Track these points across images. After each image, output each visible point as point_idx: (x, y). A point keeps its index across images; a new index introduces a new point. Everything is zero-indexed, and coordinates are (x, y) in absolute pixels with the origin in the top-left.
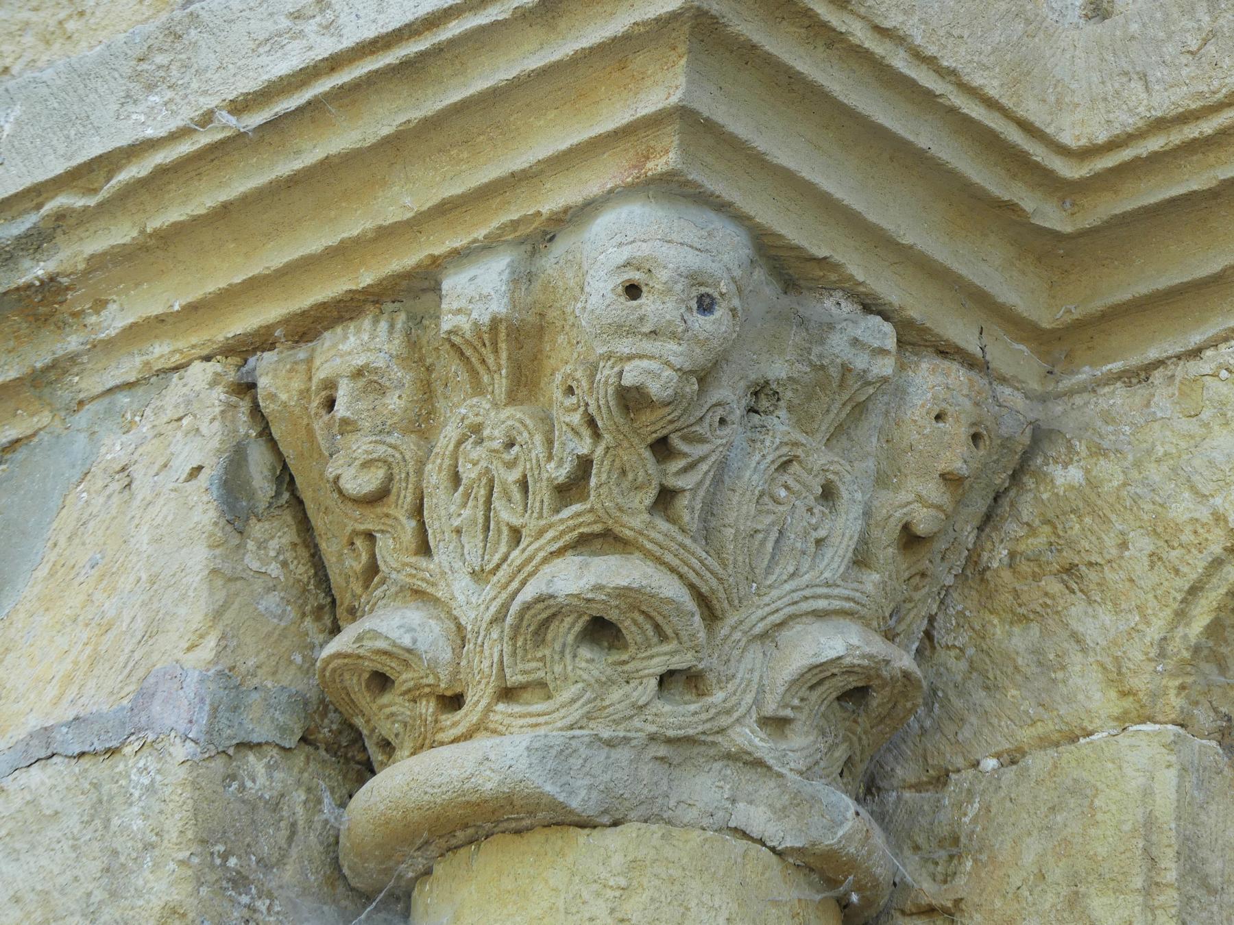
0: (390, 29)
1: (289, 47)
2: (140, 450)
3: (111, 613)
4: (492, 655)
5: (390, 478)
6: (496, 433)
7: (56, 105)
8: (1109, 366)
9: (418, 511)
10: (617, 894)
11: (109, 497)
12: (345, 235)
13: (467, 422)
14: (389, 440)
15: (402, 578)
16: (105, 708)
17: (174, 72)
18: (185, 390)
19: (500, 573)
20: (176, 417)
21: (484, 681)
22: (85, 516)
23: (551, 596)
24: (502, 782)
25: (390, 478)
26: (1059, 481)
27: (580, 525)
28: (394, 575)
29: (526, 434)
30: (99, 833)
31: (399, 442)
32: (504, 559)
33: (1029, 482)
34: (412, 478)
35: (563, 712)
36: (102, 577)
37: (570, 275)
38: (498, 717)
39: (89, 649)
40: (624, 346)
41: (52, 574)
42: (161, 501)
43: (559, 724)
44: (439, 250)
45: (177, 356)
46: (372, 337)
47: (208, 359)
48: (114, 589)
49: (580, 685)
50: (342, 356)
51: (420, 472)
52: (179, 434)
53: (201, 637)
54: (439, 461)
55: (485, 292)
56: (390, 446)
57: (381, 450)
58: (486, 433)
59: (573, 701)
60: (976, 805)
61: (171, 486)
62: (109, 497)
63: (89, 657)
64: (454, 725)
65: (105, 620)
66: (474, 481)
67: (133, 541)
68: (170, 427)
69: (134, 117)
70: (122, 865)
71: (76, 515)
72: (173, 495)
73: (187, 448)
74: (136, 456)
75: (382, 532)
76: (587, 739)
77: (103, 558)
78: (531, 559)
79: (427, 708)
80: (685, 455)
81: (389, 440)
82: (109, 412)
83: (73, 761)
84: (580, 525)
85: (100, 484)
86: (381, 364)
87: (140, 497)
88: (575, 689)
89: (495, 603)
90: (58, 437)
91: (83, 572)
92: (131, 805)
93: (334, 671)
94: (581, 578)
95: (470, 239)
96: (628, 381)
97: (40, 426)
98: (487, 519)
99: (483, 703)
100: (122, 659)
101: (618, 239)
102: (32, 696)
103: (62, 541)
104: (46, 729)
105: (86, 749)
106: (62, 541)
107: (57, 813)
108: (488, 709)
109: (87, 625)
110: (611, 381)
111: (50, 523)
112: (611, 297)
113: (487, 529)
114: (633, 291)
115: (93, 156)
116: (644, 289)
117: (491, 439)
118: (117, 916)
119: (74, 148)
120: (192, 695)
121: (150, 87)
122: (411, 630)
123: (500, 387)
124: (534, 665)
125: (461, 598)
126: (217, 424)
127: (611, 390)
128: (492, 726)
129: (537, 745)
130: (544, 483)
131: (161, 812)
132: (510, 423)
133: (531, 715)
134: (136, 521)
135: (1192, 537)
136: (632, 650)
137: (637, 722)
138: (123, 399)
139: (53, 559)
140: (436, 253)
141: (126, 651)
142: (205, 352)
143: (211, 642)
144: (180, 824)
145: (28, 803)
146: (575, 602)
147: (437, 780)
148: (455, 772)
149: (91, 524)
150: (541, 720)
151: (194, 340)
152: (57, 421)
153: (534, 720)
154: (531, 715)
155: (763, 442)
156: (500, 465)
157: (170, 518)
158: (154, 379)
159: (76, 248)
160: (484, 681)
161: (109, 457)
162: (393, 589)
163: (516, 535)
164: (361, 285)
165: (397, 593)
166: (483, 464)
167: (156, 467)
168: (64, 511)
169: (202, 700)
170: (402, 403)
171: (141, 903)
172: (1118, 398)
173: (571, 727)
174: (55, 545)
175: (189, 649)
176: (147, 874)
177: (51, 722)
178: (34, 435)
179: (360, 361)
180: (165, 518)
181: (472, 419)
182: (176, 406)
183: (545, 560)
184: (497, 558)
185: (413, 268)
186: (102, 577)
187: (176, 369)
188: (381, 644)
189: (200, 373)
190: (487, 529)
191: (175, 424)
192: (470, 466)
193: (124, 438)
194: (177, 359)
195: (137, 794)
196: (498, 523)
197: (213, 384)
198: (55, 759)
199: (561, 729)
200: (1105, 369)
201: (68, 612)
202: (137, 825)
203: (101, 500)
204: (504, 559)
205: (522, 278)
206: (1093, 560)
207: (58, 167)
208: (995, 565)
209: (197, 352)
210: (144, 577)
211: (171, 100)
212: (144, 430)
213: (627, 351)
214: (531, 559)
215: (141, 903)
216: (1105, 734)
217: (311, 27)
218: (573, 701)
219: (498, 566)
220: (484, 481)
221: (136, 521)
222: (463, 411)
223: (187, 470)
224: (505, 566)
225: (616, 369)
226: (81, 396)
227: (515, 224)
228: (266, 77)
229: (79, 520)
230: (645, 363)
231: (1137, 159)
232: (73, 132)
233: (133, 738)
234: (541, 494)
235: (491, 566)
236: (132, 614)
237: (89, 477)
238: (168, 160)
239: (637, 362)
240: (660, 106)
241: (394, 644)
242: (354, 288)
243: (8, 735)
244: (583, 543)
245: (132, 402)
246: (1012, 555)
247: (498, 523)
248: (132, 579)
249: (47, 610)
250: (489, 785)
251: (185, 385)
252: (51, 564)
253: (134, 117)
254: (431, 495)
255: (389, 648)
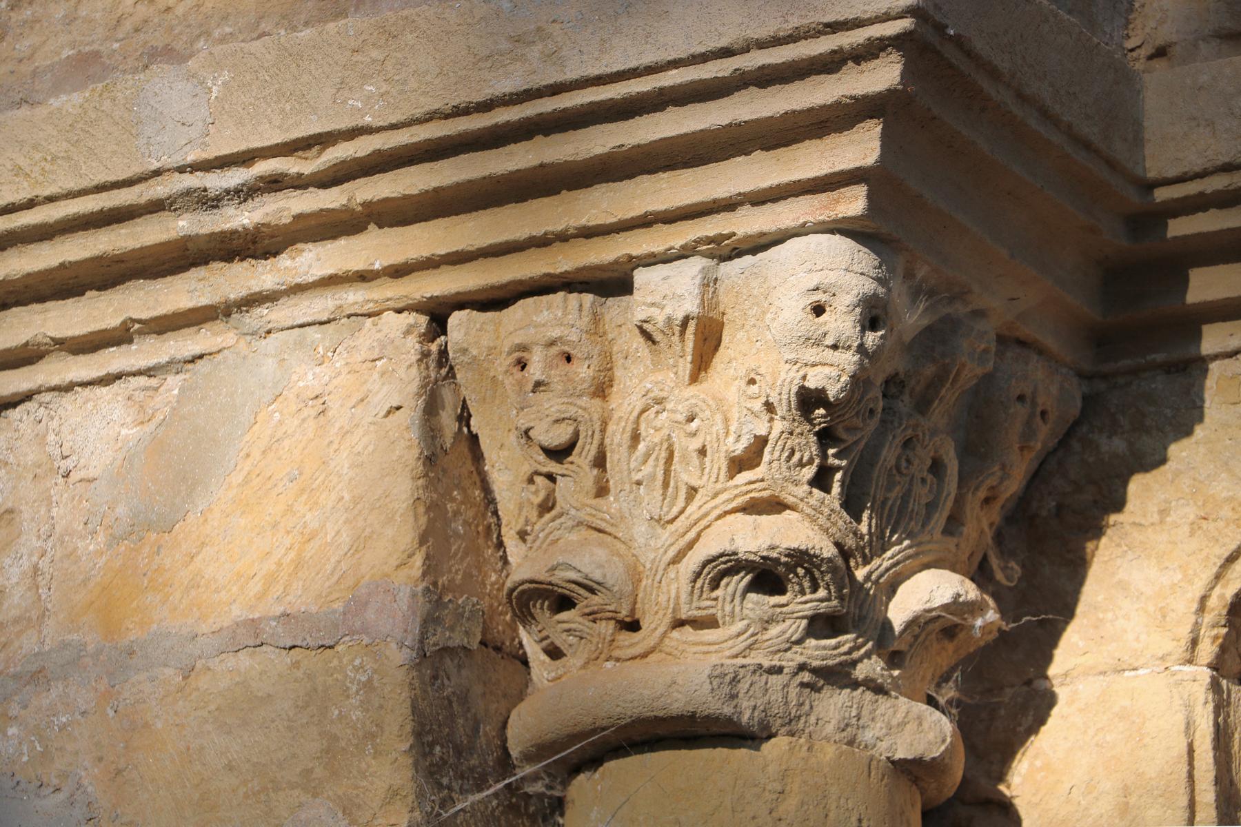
0: (615, 70)
1: (511, 68)
2: (335, 382)
3: (314, 525)
4: (669, 591)
5: (576, 434)
6: (680, 407)
7: (268, 78)
8: (1153, 356)
9: (600, 461)
10: (774, 797)
11: (304, 420)
12: (550, 228)
13: (652, 395)
14: (579, 402)
15: (582, 515)
16: (314, 609)
17: (390, 68)
18: (379, 335)
19: (678, 523)
20: (372, 357)
21: (661, 613)
22: (279, 434)
23: (735, 553)
24: (688, 703)
25: (576, 434)
26: (1104, 448)
27: (751, 491)
28: (573, 512)
29: (708, 413)
30: (316, 719)
31: (588, 405)
32: (682, 512)
33: (1076, 445)
34: (597, 436)
35: (730, 643)
36: (302, 491)
37: (754, 284)
38: (674, 644)
39: (292, 555)
40: (810, 354)
41: (246, 481)
42: (360, 431)
43: (727, 653)
44: (636, 252)
45: (371, 305)
46: (565, 314)
47: (399, 311)
48: (316, 503)
49: (745, 622)
50: (535, 327)
51: (603, 431)
52: (376, 376)
53: (410, 556)
54: (623, 424)
55: (679, 292)
56: (581, 407)
57: (572, 411)
58: (669, 406)
59: (739, 635)
60: (1030, 718)
61: (370, 419)
62: (304, 420)
63: (292, 561)
64: (632, 645)
65: (307, 531)
66: (656, 445)
67: (333, 464)
68: (364, 366)
69: (350, 102)
70: (343, 749)
71: (269, 432)
72: (372, 428)
73: (385, 388)
74: (330, 387)
75: (563, 476)
76: (752, 668)
77: (301, 474)
78: (706, 515)
79: (607, 628)
80: (842, 441)
81: (579, 402)
82: (300, 344)
83: (284, 652)
84: (751, 491)
85: (294, 408)
86: (574, 338)
87: (337, 425)
88: (740, 625)
89: (672, 548)
90: (245, 358)
91: (281, 484)
92: (348, 697)
93: (523, 592)
94: (756, 538)
95: (667, 246)
96: (811, 384)
97: (224, 345)
98: (667, 473)
99: (661, 630)
100: (329, 567)
101: (808, 266)
102: (235, 589)
103: (256, 454)
104: (253, 620)
105: (299, 643)
106: (256, 454)
107: (269, 695)
108: (664, 635)
109: (288, 532)
110: (796, 382)
111: (242, 435)
112: (801, 315)
113: (666, 484)
114: (818, 310)
115: (311, 133)
116: (828, 309)
117: (674, 411)
118: (340, 793)
119: (290, 122)
120: (405, 608)
121: (365, 78)
122: (601, 566)
123: (684, 370)
124: (709, 603)
125: (642, 541)
126: (414, 370)
127: (795, 389)
128: (668, 650)
129: (715, 673)
130: (723, 455)
131: (381, 707)
132: (693, 401)
133: (703, 644)
134: (335, 446)
135: (1230, 514)
136: (789, 595)
137: (789, 654)
138: (313, 333)
139: (247, 469)
140: (634, 254)
141: (333, 560)
142: (400, 305)
143: (418, 560)
144: (400, 719)
145: (238, 683)
146: (752, 557)
147: (630, 697)
148: (646, 692)
149: (287, 442)
150: (712, 648)
151: (389, 294)
152: (242, 343)
153: (705, 648)
154: (703, 644)
155: (892, 422)
156: (682, 434)
157: (371, 448)
158: (345, 320)
159: (282, 204)
160: (661, 613)
161: (301, 384)
162: (570, 523)
163: (693, 491)
164: (559, 271)
165: (573, 527)
166: (665, 431)
167: (354, 401)
168: (256, 427)
169: (414, 613)
170: (591, 372)
171: (365, 783)
172: (1159, 384)
173: (736, 656)
174: (248, 455)
175: (398, 567)
176: (369, 759)
177: (256, 615)
178: (219, 352)
179: (555, 333)
180: (366, 448)
181: (656, 393)
182: (372, 348)
183: (719, 517)
184: (675, 510)
185: (610, 263)
186: (302, 491)
187: (369, 315)
188: (573, 575)
189: (394, 323)
190: (666, 484)
191: (370, 365)
192: (652, 431)
193: (318, 369)
194: (370, 307)
195: (354, 688)
196: (676, 482)
197: (407, 332)
198: (264, 647)
199: (729, 657)
200: (1149, 358)
201: (267, 518)
202: (356, 715)
203: (296, 422)
204: (682, 512)
205: (709, 284)
206: (1137, 521)
207: (277, 138)
208: (1044, 513)
209: (391, 304)
210: (347, 497)
211: (387, 92)
212: (338, 365)
213: (812, 359)
214: (706, 515)
215: (365, 783)
216: (1148, 671)
217: (535, 52)
218: (739, 635)
219: (676, 517)
220: (665, 445)
221: (335, 446)
222: (649, 386)
223: (386, 408)
224: (682, 517)
225: (802, 373)
226: (270, 326)
227: (710, 240)
228: (491, 91)
229: (272, 436)
230: (827, 370)
231: (1201, 194)
232: (288, 107)
233: (347, 638)
234: (718, 463)
235: (670, 517)
236: (336, 528)
237: (280, 399)
238: (386, 147)
239: (819, 369)
240: (857, 164)
241: (586, 577)
242: (552, 271)
243: (211, 621)
244: (754, 507)
245: (323, 339)
246: (1060, 507)
247: (676, 482)
248: (334, 496)
249: (244, 512)
250: (676, 705)
251: (380, 331)
252: (244, 472)
253: (350, 102)
254: (612, 451)
255: (581, 580)
